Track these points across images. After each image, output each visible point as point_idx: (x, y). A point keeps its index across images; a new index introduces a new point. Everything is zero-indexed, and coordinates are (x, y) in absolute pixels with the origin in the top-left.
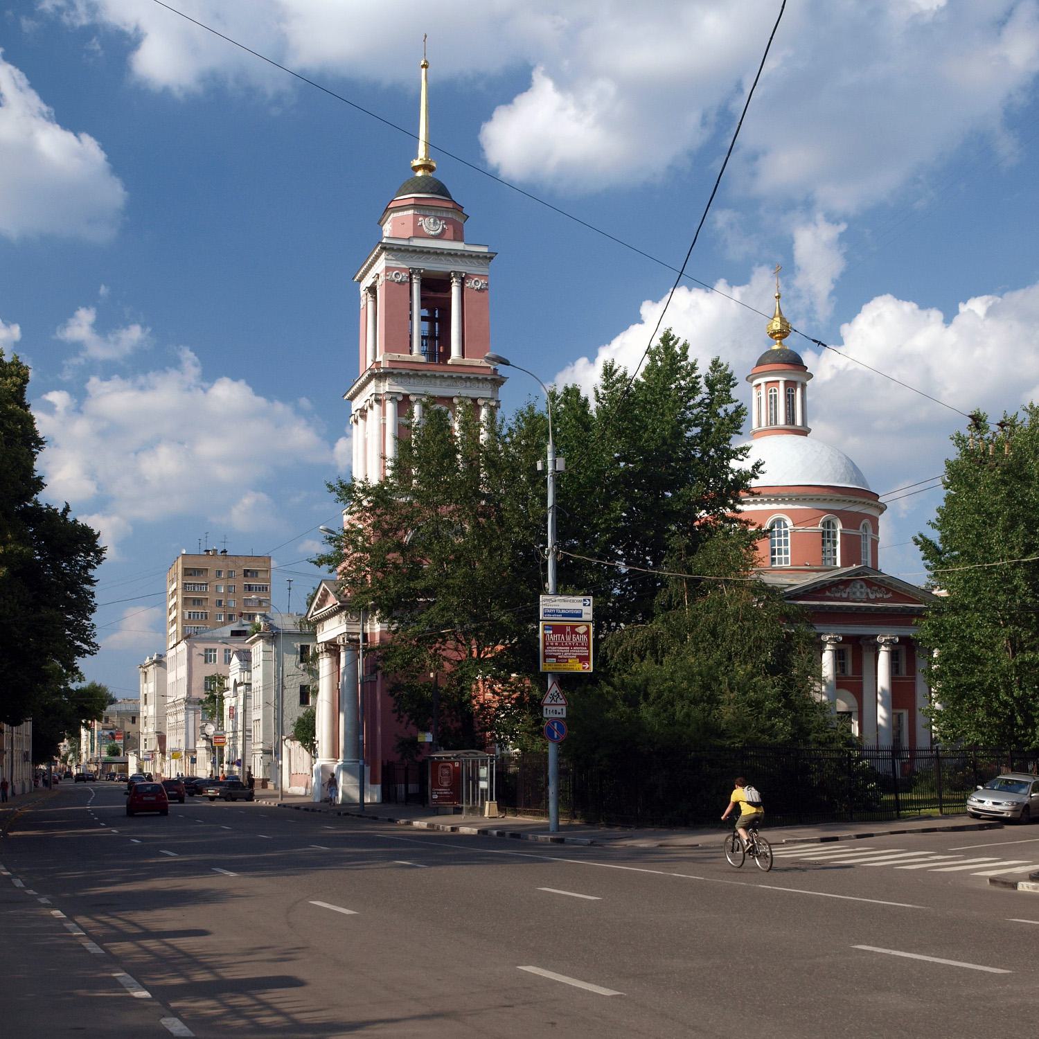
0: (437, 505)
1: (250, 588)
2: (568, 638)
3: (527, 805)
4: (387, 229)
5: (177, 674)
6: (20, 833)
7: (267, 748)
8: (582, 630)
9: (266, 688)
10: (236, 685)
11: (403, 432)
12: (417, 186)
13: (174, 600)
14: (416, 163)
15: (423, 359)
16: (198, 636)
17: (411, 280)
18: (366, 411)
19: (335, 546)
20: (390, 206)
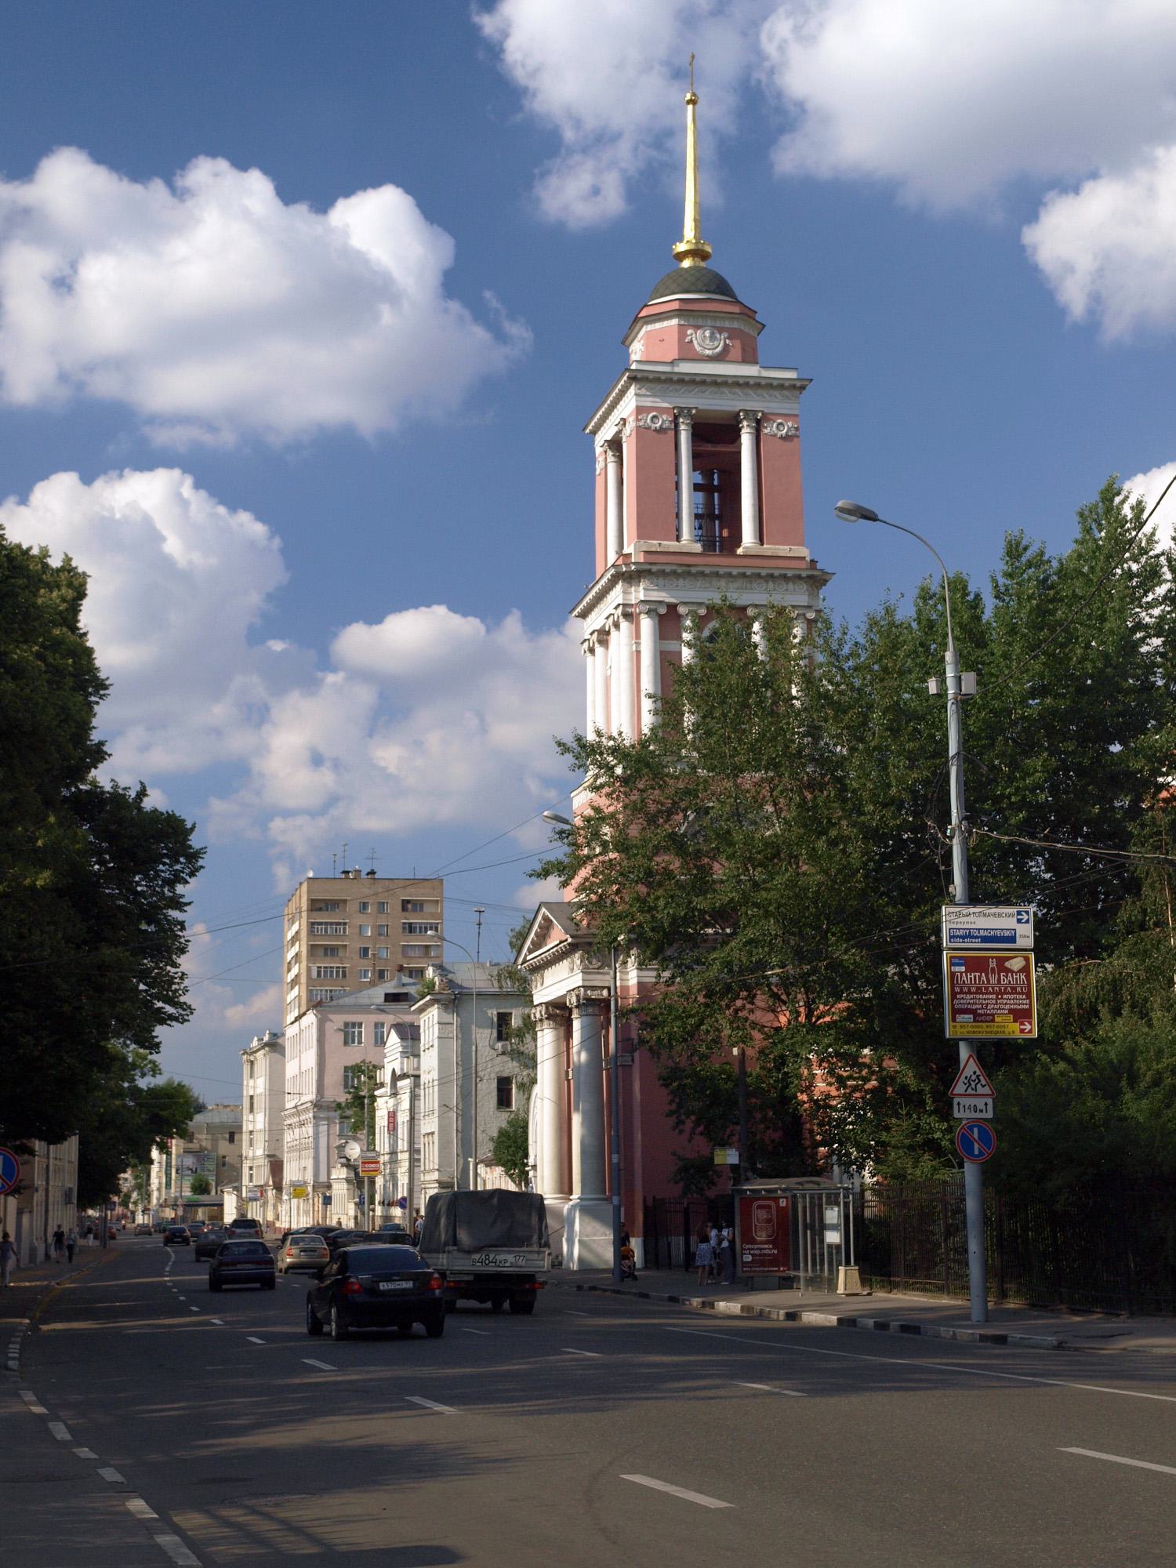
0: (738, 770)
1: (411, 928)
2: (994, 980)
3: (912, 1270)
4: (637, 350)
5: (301, 1063)
6: (59, 1326)
7: (445, 1179)
8: (1016, 964)
9: (443, 1081)
10: (395, 1078)
11: (666, 662)
12: (684, 281)
13: (295, 949)
14: (681, 247)
15: (698, 548)
16: (334, 1003)
17: (677, 425)
18: (608, 633)
19: (569, 845)
20: (643, 314)
